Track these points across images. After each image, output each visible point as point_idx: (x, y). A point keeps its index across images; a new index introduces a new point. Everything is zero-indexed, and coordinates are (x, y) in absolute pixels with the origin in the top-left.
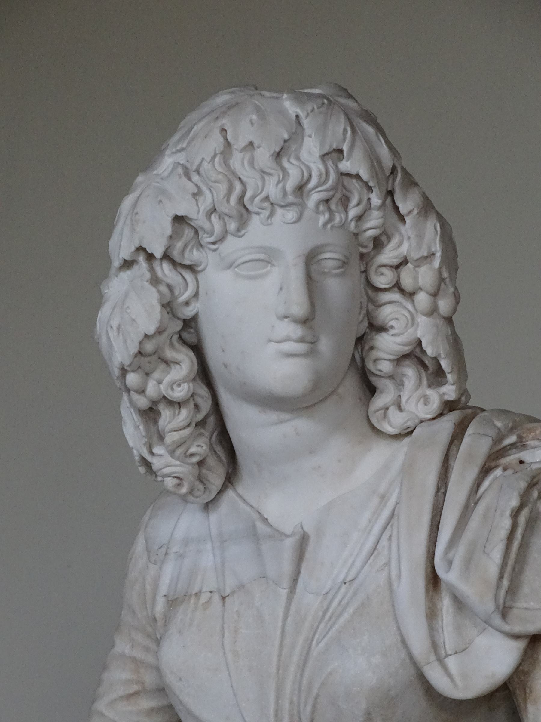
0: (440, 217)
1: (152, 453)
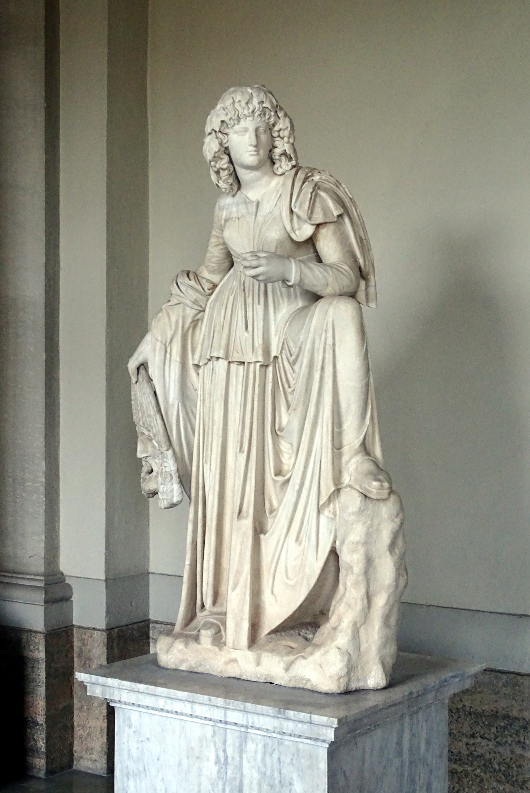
0: (289, 117)
1: (218, 182)
